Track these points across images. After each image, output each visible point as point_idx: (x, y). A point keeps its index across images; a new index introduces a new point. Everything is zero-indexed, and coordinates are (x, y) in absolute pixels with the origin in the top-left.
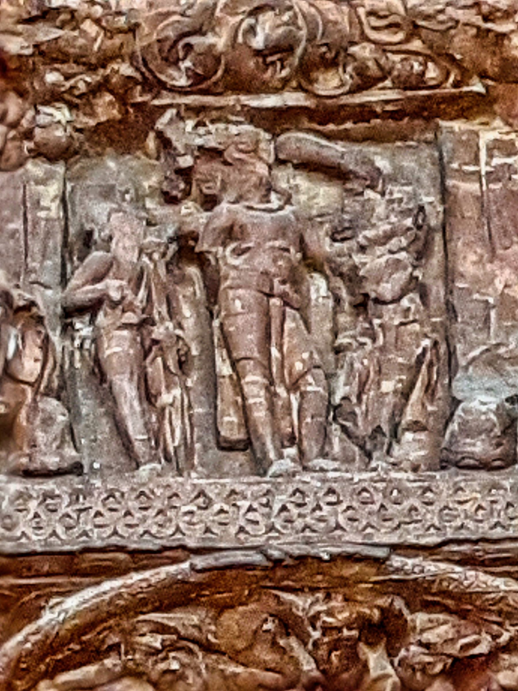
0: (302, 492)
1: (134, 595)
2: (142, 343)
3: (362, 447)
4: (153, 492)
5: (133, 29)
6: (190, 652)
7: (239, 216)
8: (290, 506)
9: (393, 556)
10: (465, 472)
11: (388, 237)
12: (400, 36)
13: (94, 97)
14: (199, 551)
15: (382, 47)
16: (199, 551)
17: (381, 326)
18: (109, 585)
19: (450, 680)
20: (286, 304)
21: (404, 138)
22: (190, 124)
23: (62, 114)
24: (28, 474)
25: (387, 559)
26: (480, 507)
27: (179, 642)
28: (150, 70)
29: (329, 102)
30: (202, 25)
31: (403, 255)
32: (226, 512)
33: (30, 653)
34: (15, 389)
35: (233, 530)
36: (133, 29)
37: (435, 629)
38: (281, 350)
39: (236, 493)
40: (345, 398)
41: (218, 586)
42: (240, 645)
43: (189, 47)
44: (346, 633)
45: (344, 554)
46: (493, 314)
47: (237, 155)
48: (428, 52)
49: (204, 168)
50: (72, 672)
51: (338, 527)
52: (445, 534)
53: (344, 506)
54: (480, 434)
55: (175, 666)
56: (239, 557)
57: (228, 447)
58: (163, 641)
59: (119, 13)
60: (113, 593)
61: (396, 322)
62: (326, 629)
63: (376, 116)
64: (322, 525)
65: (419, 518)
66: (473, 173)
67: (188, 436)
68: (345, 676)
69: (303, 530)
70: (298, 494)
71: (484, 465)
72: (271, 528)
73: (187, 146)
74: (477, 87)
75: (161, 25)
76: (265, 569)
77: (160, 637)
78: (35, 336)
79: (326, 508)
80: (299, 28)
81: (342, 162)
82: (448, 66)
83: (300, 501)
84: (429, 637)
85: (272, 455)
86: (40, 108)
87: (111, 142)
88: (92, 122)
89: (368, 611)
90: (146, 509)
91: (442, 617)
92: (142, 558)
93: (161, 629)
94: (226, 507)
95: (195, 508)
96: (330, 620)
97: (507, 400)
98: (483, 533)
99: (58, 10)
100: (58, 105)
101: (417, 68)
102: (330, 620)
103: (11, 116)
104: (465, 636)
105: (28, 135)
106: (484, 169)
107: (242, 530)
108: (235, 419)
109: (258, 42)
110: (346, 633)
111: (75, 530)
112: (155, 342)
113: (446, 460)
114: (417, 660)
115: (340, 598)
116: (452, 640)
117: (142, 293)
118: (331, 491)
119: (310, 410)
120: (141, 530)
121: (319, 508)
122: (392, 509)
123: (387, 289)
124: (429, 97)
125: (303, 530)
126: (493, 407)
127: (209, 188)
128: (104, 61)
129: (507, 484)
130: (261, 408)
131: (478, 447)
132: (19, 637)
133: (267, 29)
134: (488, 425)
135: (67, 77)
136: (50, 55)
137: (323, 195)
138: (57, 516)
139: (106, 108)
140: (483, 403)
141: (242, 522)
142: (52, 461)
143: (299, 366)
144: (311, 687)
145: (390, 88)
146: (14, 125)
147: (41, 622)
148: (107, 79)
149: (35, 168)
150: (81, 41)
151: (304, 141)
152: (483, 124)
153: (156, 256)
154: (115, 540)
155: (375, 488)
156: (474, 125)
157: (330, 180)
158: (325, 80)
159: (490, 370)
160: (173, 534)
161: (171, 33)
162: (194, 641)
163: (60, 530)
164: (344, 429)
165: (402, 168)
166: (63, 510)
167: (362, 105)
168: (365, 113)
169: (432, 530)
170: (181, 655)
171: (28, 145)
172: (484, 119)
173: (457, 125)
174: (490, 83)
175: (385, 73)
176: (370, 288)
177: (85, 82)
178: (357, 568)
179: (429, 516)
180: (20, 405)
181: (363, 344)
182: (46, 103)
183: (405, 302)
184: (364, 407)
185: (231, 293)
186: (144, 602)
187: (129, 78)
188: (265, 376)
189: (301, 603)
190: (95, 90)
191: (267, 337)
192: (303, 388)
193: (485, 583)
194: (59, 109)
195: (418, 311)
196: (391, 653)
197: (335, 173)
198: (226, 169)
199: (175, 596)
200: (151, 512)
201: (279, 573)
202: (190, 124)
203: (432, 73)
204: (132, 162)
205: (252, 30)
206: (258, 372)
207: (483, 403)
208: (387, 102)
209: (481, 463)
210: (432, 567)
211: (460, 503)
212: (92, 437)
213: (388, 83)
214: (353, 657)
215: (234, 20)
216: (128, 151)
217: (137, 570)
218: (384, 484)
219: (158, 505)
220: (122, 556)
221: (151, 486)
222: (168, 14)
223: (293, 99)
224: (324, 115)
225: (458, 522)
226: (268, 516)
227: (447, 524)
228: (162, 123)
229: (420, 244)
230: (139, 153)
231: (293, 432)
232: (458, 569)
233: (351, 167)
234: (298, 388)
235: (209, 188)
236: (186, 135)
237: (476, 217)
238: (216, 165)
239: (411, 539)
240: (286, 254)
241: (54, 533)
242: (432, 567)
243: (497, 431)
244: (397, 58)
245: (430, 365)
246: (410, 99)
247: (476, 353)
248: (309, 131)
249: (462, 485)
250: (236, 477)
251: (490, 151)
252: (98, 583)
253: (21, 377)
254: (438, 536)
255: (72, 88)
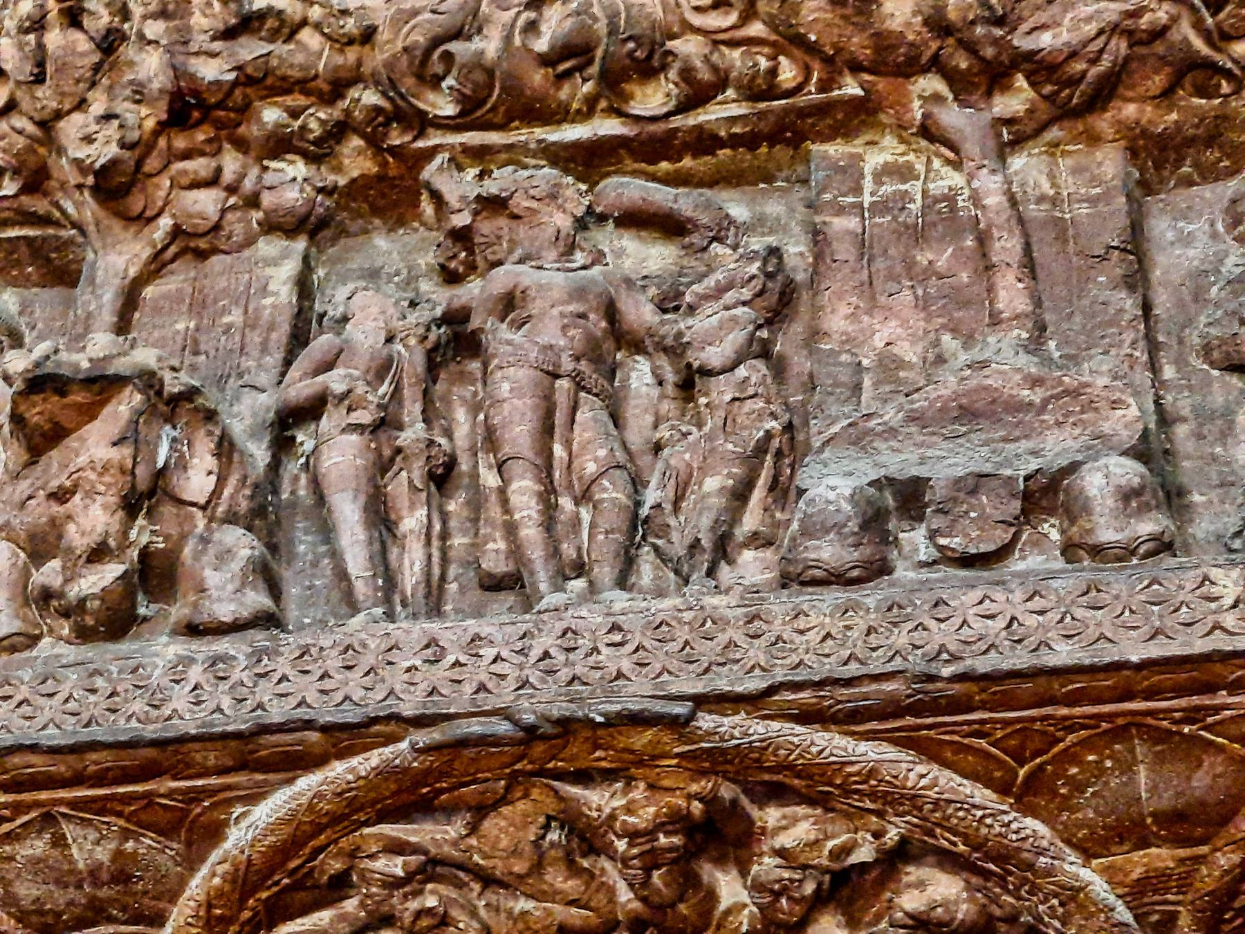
0: (575, 633)
1: (340, 794)
2: (378, 450)
3: (677, 572)
4: (365, 646)
5: (368, 36)
6: (460, 885)
7: (521, 279)
8: (552, 651)
9: (700, 714)
10: (810, 589)
11: (721, 290)
12: (733, 18)
13: (338, 142)
14: (420, 722)
15: (716, 40)
16: (420, 722)
17: (707, 405)
18: (308, 783)
19: (832, 906)
20: (580, 386)
21: (769, 179)
22: (472, 172)
23: (297, 168)
24: (193, 630)
25: (691, 717)
26: (828, 635)
27: (431, 868)
28: (402, 96)
29: (652, 128)
30: (463, 27)
31: (740, 311)
32: (462, 665)
33: (220, 893)
34: (178, 515)
35: (468, 689)
36: (368, 36)
37: (791, 827)
38: (568, 444)
39: (481, 639)
40: (658, 506)
41: (452, 772)
42: (519, 867)
43: (448, 57)
44: (663, 840)
45: (625, 712)
46: (867, 382)
47: (526, 204)
48: (774, 37)
49: (486, 227)
50: (299, 921)
51: (620, 675)
52: (773, 677)
53: (630, 648)
54: (827, 532)
55: (431, 902)
56: (475, 727)
57: (494, 585)
58: (405, 864)
59: (345, 13)
60: (310, 794)
61: (728, 398)
62: (633, 835)
63: (722, 143)
64: (598, 674)
65: (738, 656)
66: (853, 205)
67: (436, 571)
68: (683, 908)
69: (570, 683)
70: (569, 635)
71: (836, 578)
72: (524, 684)
73: (463, 198)
74: (851, 88)
75: (405, 30)
76: (512, 742)
77: (400, 860)
78: (206, 440)
79: (605, 651)
80: (596, 19)
81: (675, 207)
82: (807, 58)
83: (572, 644)
84: (785, 840)
85: (543, 587)
86: (265, 162)
87: (376, 211)
88: (342, 181)
89: (682, 803)
90: (349, 668)
91: (801, 810)
92: (346, 737)
93: (397, 848)
94: (463, 659)
95: (418, 663)
96: (631, 820)
97: (870, 484)
98: (830, 671)
99: (262, 15)
100: (288, 157)
101: (764, 63)
102: (631, 820)
103: (228, 176)
104: (833, 837)
105: (253, 201)
106: (867, 199)
107: (482, 688)
108: (502, 545)
109: (541, 45)
110: (663, 840)
111: (249, 702)
112: (399, 451)
113: (793, 578)
114: (772, 877)
115: (642, 785)
116: (817, 841)
117: (385, 388)
118: (615, 628)
119: (603, 525)
120: (338, 697)
121: (595, 650)
122: (702, 647)
123: (714, 356)
124: (786, 110)
125: (570, 683)
126: (848, 492)
127: (494, 253)
128: (338, 87)
129: (871, 602)
130: (530, 523)
131: (827, 552)
132: (204, 870)
133: (554, 25)
134: (840, 518)
135: (294, 114)
136: (259, 82)
137: (652, 256)
138: (224, 686)
139: (355, 160)
140: (833, 489)
141: (484, 677)
142: (225, 612)
143: (591, 468)
144: (637, 925)
145: (734, 101)
146: (232, 189)
147: (227, 845)
148: (348, 112)
149: (267, 247)
150: (299, 58)
151: (627, 188)
152: (867, 143)
153: (412, 341)
154: (303, 713)
155: (680, 621)
156: (856, 147)
157: (669, 238)
158: (645, 95)
159: (852, 451)
160: (384, 700)
161: (419, 38)
162: (460, 867)
163: (226, 702)
164: (656, 549)
165: (764, 218)
166: (236, 675)
167: (699, 128)
168: (704, 142)
169: (757, 672)
170: (443, 889)
171: (256, 215)
172: (868, 137)
173: (835, 149)
174: (866, 77)
175: (722, 81)
176: (696, 358)
177: (319, 119)
178: (649, 734)
179: (751, 653)
180: (183, 537)
181: (685, 435)
182: (275, 156)
183: (742, 372)
184: (682, 519)
185: (499, 374)
186: (354, 805)
187: (377, 110)
188: (540, 481)
189: (598, 800)
190: (339, 131)
191: (547, 429)
192: (597, 497)
193: (845, 750)
194: (292, 162)
195: (763, 383)
196: (744, 873)
197: (668, 226)
198: (514, 223)
199: (406, 796)
200: (357, 674)
201: (539, 749)
202: (472, 172)
203: (788, 73)
204: (408, 237)
205: (532, 28)
206: (529, 475)
207: (833, 489)
208: (733, 120)
209: (833, 575)
210: (759, 729)
211: (802, 632)
212: (307, 583)
213: (730, 93)
214: (688, 882)
215: (508, 16)
216: (401, 222)
217: (342, 755)
218: (692, 613)
219: (368, 660)
220: (314, 736)
221: (363, 636)
222: (415, 13)
223: (609, 127)
224: (649, 148)
225: (795, 659)
226: (521, 667)
227: (779, 662)
228: (429, 172)
229: (772, 299)
230: (416, 224)
231: (580, 556)
232: (799, 729)
233: (689, 214)
234: (590, 499)
235: (494, 253)
236: (460, 187)
237: (852, 259)
238: (503, 222)
239: (723, 685)
240: (582, 321)
241: (219, 710)
242: (759, 729)
243: (853, 526)
244: (736, 54)
245: (779, 454)
246: (761, 115)
247: (836, 429)
248: (635, 173)
249: (805, 607)
250: (498, 623)
251: (878, 177)
252: (290, 781)
253: (186, 497)
254: (762, 678)
255: (303, 128)
